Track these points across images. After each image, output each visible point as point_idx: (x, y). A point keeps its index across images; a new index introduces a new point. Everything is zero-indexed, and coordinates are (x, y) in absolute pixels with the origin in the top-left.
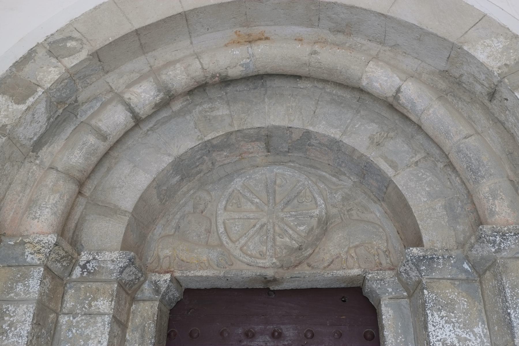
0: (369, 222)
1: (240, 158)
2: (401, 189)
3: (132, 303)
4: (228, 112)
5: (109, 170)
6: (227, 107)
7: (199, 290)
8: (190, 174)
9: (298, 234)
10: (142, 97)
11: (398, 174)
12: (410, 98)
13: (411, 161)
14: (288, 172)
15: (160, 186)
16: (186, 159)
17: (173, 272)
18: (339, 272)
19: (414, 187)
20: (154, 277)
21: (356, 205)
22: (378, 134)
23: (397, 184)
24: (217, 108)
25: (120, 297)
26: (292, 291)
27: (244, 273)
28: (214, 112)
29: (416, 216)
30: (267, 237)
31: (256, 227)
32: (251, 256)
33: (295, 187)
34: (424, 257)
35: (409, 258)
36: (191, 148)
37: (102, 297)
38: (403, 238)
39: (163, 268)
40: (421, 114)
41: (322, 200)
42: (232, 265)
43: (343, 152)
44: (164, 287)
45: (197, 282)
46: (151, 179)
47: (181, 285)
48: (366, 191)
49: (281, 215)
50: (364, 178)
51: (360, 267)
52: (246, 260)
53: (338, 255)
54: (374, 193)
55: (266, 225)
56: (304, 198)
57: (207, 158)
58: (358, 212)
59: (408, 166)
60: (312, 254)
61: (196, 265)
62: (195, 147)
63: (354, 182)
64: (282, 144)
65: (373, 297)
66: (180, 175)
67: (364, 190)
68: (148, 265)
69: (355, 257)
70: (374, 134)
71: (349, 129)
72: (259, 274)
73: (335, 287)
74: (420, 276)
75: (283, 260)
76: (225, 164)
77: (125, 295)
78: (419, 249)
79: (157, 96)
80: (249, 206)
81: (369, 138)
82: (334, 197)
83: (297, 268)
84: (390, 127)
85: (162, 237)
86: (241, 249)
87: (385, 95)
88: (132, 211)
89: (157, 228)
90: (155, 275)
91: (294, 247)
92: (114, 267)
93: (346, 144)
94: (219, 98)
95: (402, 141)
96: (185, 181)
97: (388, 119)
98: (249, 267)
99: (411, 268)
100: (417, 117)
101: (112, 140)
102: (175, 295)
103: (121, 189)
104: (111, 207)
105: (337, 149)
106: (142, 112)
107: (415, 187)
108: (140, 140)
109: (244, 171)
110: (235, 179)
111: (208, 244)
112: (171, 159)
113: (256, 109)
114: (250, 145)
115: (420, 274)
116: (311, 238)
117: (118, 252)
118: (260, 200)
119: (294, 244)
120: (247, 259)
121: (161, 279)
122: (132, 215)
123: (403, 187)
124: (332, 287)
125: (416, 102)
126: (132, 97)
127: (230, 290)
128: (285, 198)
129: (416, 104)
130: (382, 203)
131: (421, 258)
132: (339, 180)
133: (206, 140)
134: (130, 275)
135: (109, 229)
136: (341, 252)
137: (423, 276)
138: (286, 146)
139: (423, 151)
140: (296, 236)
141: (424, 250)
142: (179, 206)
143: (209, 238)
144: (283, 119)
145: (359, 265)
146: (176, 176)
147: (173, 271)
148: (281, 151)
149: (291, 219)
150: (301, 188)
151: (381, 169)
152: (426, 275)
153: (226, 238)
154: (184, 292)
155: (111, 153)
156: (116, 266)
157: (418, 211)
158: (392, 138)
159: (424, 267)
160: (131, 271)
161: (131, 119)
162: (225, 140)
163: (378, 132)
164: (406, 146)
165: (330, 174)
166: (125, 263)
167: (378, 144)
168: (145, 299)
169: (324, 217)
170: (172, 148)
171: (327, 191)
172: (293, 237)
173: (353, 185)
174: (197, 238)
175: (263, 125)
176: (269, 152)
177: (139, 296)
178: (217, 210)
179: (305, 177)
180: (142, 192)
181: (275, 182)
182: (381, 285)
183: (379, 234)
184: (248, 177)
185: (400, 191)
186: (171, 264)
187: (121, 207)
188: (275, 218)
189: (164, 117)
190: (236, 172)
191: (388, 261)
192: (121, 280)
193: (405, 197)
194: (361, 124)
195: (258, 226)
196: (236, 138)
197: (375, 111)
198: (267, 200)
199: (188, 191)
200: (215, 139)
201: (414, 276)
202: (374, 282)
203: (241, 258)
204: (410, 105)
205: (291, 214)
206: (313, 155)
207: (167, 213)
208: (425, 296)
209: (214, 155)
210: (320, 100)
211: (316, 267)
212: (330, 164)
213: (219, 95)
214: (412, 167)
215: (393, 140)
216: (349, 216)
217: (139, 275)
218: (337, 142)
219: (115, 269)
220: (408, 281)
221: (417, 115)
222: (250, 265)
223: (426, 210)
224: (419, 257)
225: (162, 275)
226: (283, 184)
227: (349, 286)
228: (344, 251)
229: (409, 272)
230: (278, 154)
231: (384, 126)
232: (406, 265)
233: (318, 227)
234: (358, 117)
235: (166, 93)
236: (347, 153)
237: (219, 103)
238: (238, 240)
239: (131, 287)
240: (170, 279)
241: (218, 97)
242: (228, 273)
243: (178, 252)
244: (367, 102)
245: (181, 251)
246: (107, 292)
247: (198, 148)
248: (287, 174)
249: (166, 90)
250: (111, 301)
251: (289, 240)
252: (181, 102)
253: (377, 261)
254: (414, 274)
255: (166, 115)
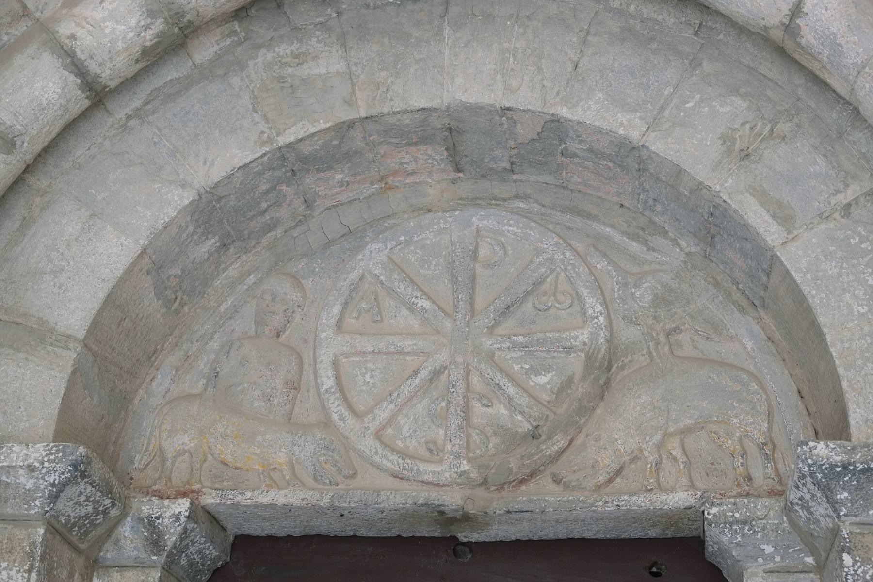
0: (722, 364)
1: (381, 188)
2: (799, 282)
3: (93, 571)
4: (341, 66)
5: (26, 224)
6: (340, 52)
7: (272, 539)
8: (246, 232)
9: (530, 395)
10: (107, 31)
11: (793, 238)
12: (826, 31)
13: (833, 202)
14: (511, 226)
15: (162, 266)
16: (230, 195)
17: (198, 493)
18: (634, 498)
19: (835, 275)
20: (148, 507)
21: (692, 317)
22: (748, 126)
23: (788, 267)
24: (313, 55)
25: (56, 559)
26: (518, 544)
27: (383, 497)
28: (305, 66)
29: (834, 354)
30: (449, 403)
31: (419, 375)
32: (403, 454)
33: (526, 267)
34: (845, 467)
35: (806, 469)
36: (241, 165)
37: (4, 561)
38: (813, 409)
39: (173, 482)
40: (856, 77)
41: (598, 305)
42: (354, 475)
43: (652, 174)
44: (173, 534)
45: (264, 519)
46: (136, 250)
47: (222, 527)
48: (719, 278)
49: (488, 343)
50: (712, 245)
51: (692, 486)
52: (389, 464)
53: (636, 453)
54: (740, 286)
55: (446, 372)
56: (552, 298)
57: (289, 189)
58: (696, 338)
59: (824, 216)
60: (565, 450)
61: (259, 475)
62: (251, 162)
63: (687, 254)
64: (492, 150)
65: (728, 565)
66: (217, 237)
67: (713, 278)
68: (134, 475)
69: (682, 459)
70: (736, 126)
71: (667, 113)
72: (424, 502)
73: (632, 536)
74: (835, 516)
75: (488, 467)
76: (341, 204)
77: (67, 553)
78: (832, 445)
79: (147, 27)
80: (404, 319)
81: (719, 138)
82: (633, 294)
83: (524, 488)
84: (780, 108)
85: (170, 402)
86: (378, 435)
87: (762, 23)
88: (86, 336)
89: (159, 377)
90: (148, 501)
91: (520, 430)
92: (35, 483)
93: (657, 155)
94: (319, 27)
95: (812, 146)
96: (231, 250)
97: (777, 84)
98: (397, 483)
99: (813, 496)
100: (845, 85)
101: (27, 149)
102: (207, 552)
103: (56, 277)
104: (31, 325)
105: (637, 166)
106: (108, 72)
107: (839, 275)
108: (107, 143)
109: (392, 222)
110: (367, 244)
111: (292, 421)
112: (187, 197)
113: (417, 57)
114: (407, 153)
115: (836, 511)
116: (565, 406)
117: (45, 444)
118: (434, 302)
119: (520, 421)
120: (393, 462)
121: (165, 512)
122: (86, 345)
123: (805, 275)
124: (625, 536)
125: (843, 43)
126: (80, 33)
127: (354, 539)
128: (499, 297)
129: (842, 47)
130: (762, 313)
131: (838, 469)
132: (648, 250)
133: (281, 144)
134: (78, 504)
135: (26, 382)
136: (645, 446)
137: (844, 518)
138: (503, 156)
139: (868, 176)
140: (523, 401)
141: (845, 447)
142: (218, 319)
143: (294, 405)
144: (489, 86)
145: (691, 480)
146: (207, 238)
147: (198, 492)
148: (491, 169)
149: (514, 355)
150: (543, 270)
151: (748, 224)
152: (851, 515)
153: (338, 405)
154: (233, 545)
155: (31, 180)
156: (41, 481)
157: (842, 342)
158: (784, 138)
159: (846, 494)
160: (81, 493)
161: (79, 92)
162: (335, 142)
163: (748, 122)
164: (821, 160)
165: (623, 233)
166: (63, 473)
167: (745, 155)
168: (125, 563)
169: (603, 351)
170: (191, 167)
171: (613, 278)
172: (517, 404)
173: (685, 263)
174: (263, 404)
175: (434, 104)
176: (458, 170)
177: (109, 556)
178: (317, 329)
179: (556, 239)
180: (110, 285)
181: (475, 252)
182: (743, 536)
183: (749, 398)
184: (402, 238)
185: (797, 286)
186: (195, 472)
187: (56, 324)
188: (472, 351)
189: (171, 80)
190: (371, 226)
191: (770, 471)
192: (56, 517)
193: (808, 303)
194: (702, 100)
195: (424, 373)
196: (364, 137)
197: (741, 63)
198: (451, 303)
199: (243, 277)
200: (307, 142)
201: (822, 516)
202: (725, 527)
203: (377, 459)
204: (826, 52)
205: (513, 343)
206: (579, 180)
207: (185, 337)
208: (846, 570)
209: (308, 181)
210: (593, 31)
211: (574, 484)
212: (625, 203)
213: (318, 20)
214: (835, 219)
215: (786, 143)
216: (670, 347)
217: (106, 503)
218: (634, 148)
219: (38, 488)
220: (812, 527)
221: (846, 79)
222: (402, 479)
223: (862, 337)
224: (832, 466)
225: (166, 502)
226: (496, 259)
227: (670, 534)
228: (651, 444)
229: (810, 505)
230: (483, 176)
231: (765, 104)
232: (801, 486)
233: (584, 378)
234: (694, 78)
235: (170, 21)
236: (663, 178)
237: (319, 42)
238: (371, 411)
239: (86, 533)
240: (187, 514)
241: (316, 25)
242: (341, 497)
243: (213, 440)
244: (721, 36)
245: (221, 439)
246: (18, 548)
247: (262, 164)
248: (508, 231)
249: (172, 13)
250: (29, 571)
251: (506, 412)
252: (216, 39)
253: (738, 471)
254: (821, 509)
255: (175, 75)
